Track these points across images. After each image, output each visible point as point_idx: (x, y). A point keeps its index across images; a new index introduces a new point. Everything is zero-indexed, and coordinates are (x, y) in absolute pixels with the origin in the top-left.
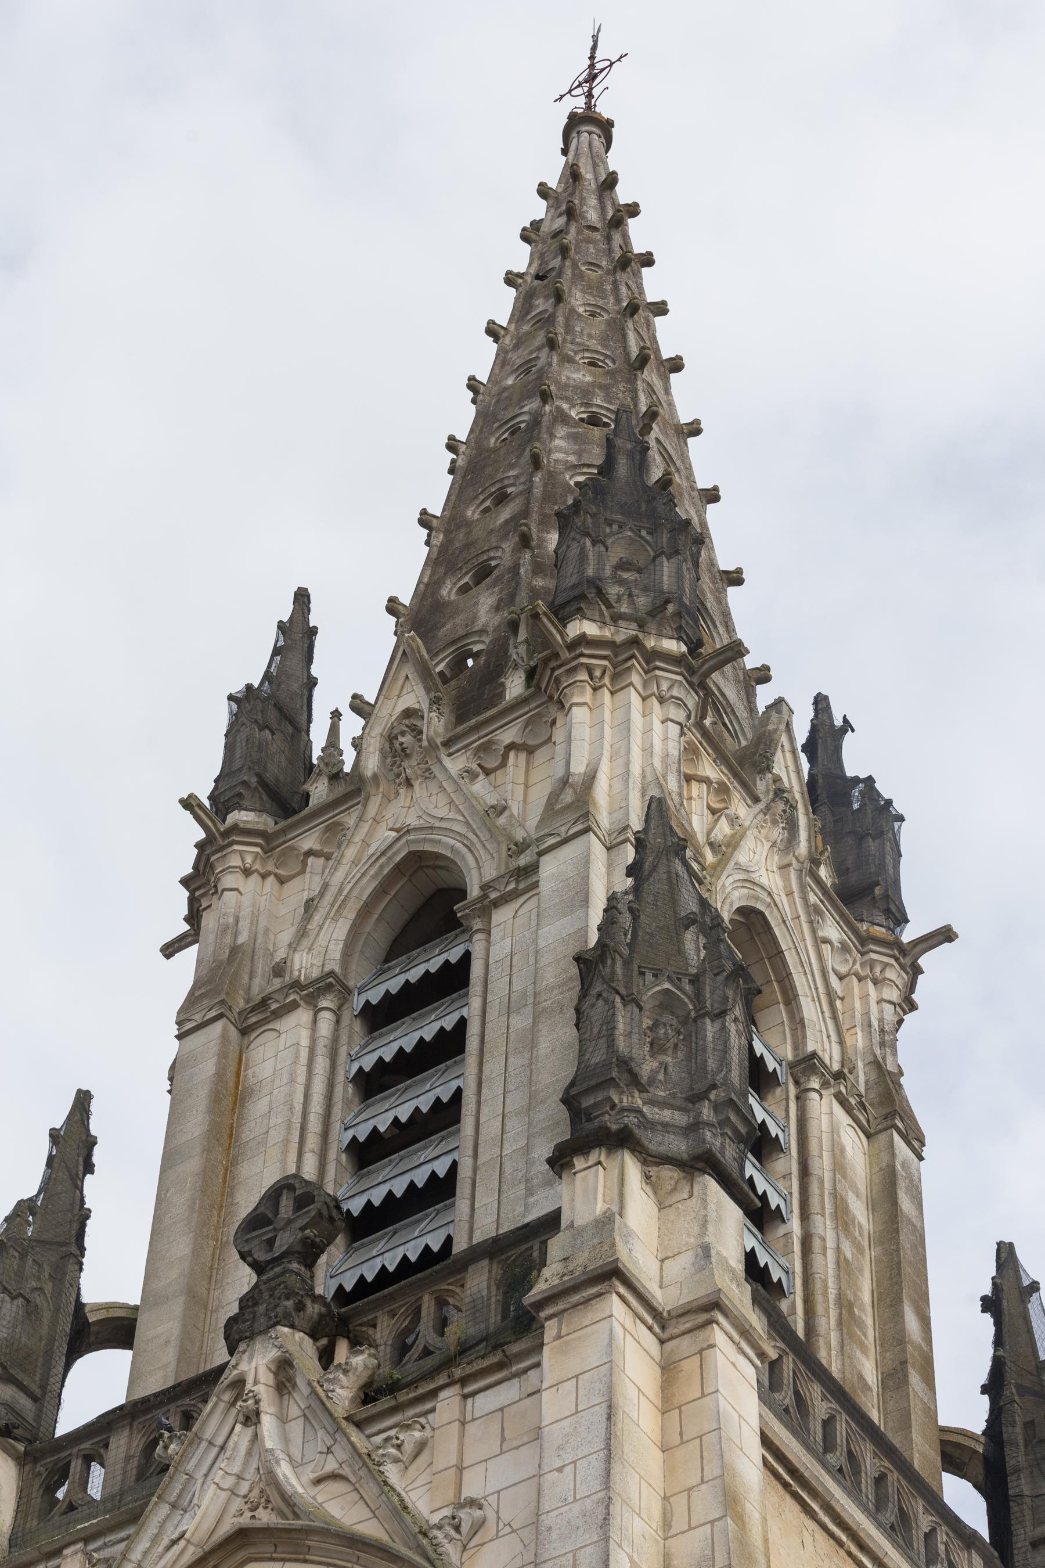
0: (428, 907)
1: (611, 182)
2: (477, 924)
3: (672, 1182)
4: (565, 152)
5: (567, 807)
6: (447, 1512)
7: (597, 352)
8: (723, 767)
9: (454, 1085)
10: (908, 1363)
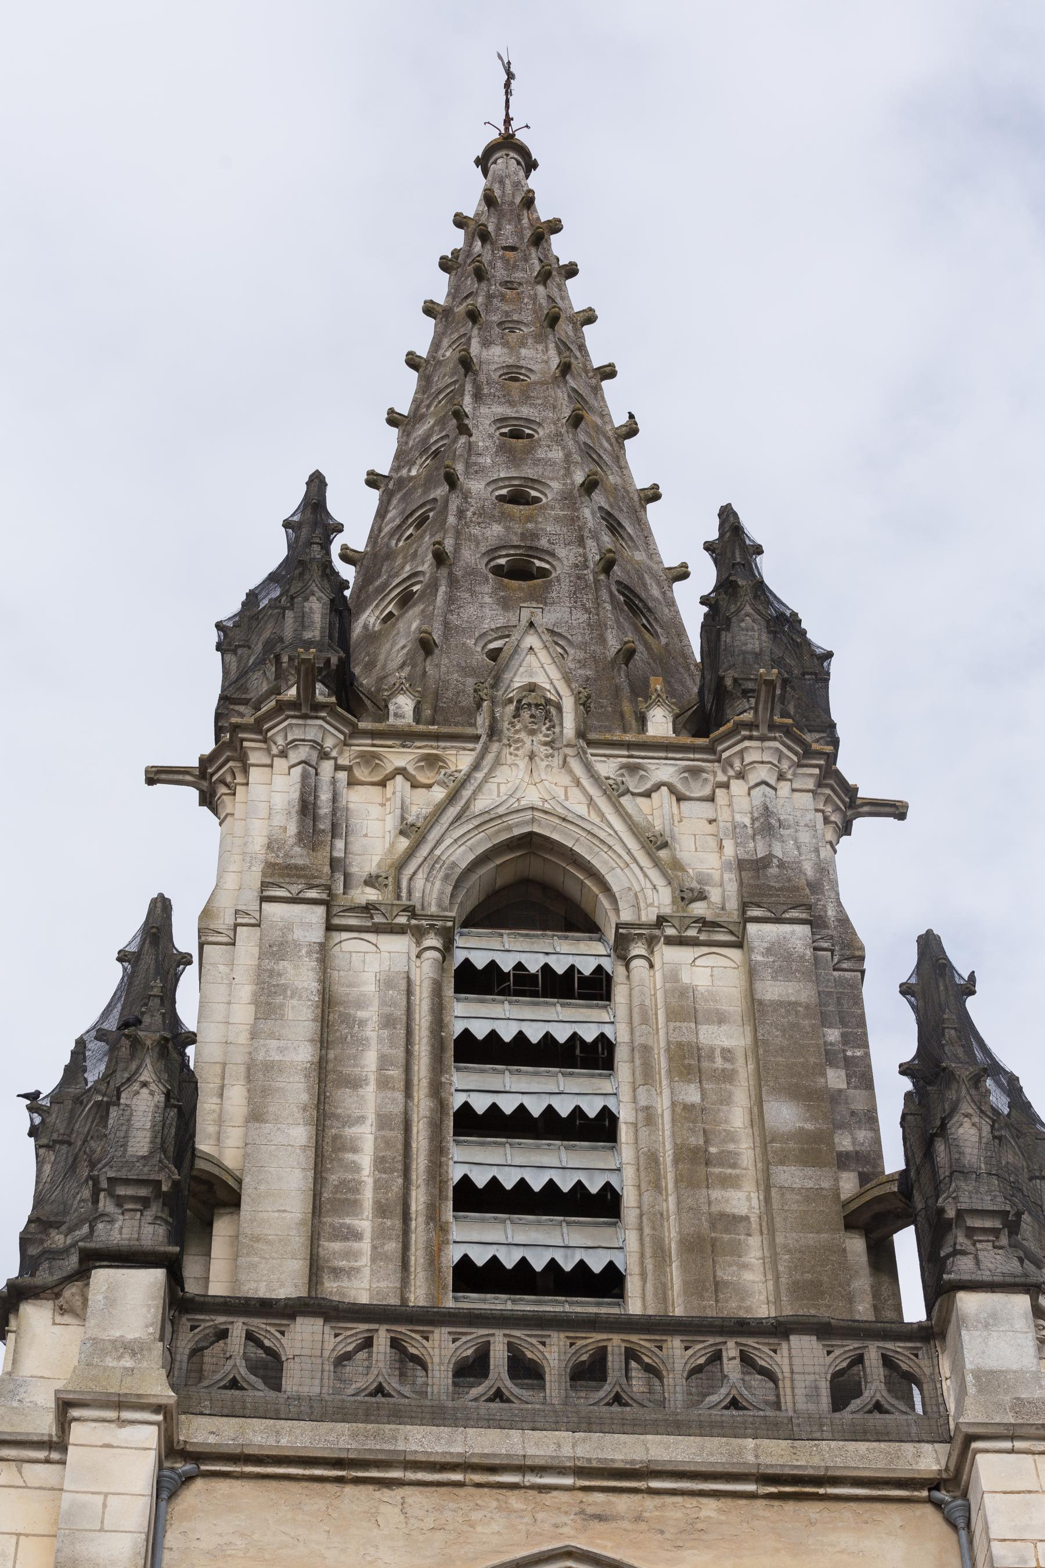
3: (77, 1297)
7: (447, 387)
8: (418, 744)
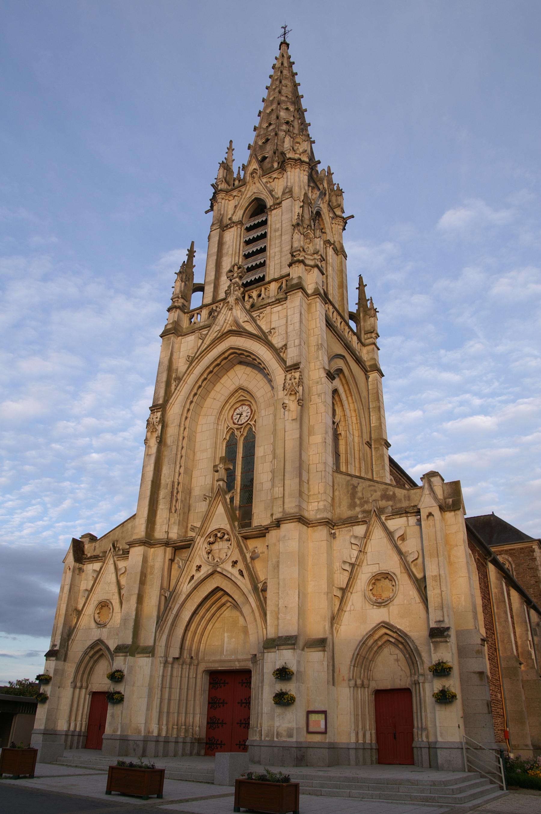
0: (259, 208)
1: (289, 57)
2: (269, 213)
4: (280, 49)
5: (287, 193)
6: (269, 330)
9: (264, 245)
10: (343, 297)
